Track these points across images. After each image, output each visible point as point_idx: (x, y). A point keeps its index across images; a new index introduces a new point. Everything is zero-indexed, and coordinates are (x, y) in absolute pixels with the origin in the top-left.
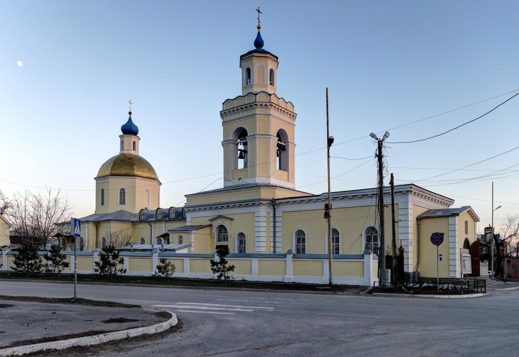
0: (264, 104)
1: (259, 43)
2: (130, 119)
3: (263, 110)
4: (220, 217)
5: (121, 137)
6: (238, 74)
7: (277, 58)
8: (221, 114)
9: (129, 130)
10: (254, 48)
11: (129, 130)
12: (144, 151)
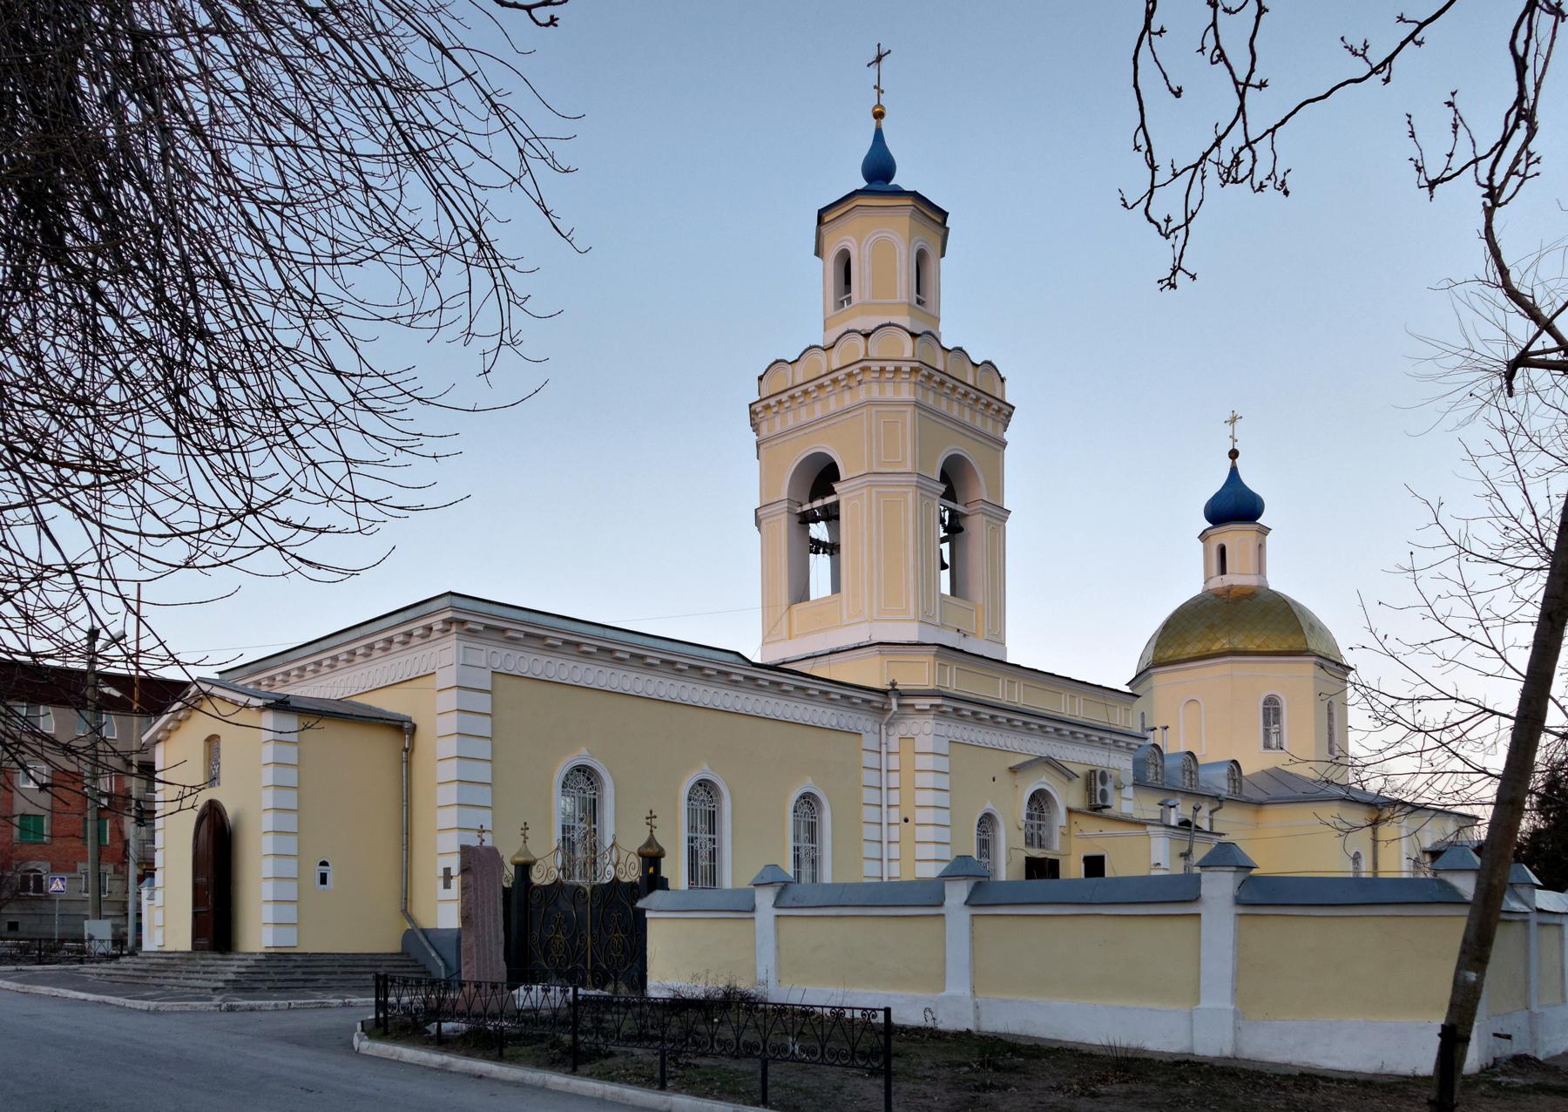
0: (890, 367)
1: (879, 169)
2: (1234, 471)
3: (889, 387)
4: (1049, 762)
5: (1203, 537)
6: (817, 275)
7: (945, 214)
8: (753, 413)
9: (1235, 508)
10: (862, 183)
11: (1235, 508)
12: (1289, 568)
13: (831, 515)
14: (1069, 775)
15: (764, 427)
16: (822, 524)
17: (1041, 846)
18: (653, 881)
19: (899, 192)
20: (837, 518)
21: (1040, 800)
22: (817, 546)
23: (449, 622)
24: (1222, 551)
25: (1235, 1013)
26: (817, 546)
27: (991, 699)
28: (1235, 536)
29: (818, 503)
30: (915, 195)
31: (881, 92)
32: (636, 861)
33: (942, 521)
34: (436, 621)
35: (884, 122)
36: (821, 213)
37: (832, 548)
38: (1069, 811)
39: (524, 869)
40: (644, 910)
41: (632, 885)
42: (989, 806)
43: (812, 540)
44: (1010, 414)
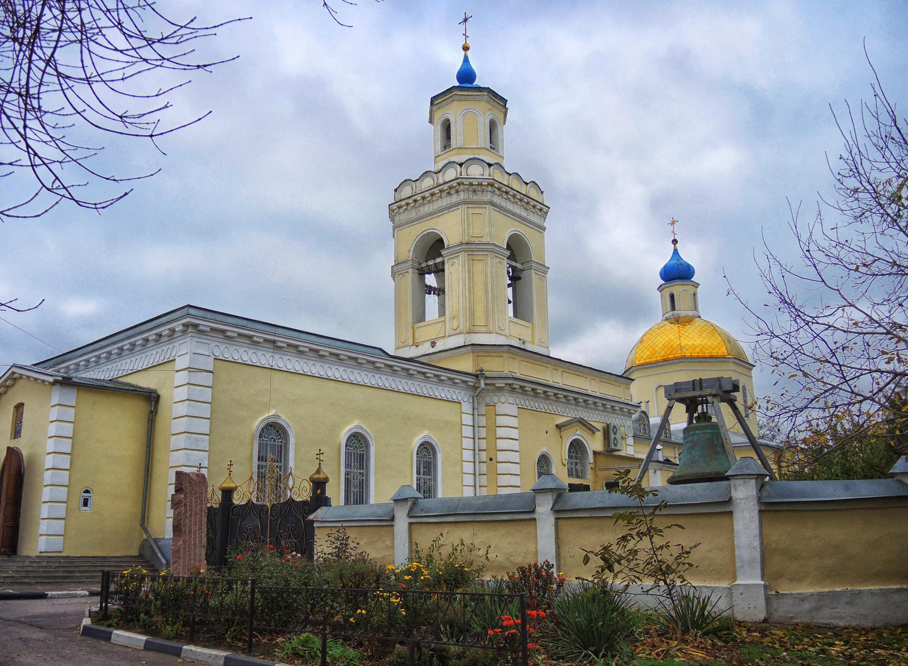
5: (660, 289)
8: (391, 211)
13: (439, 271)
14: (592, 430)
15: (397, 219)
16: (433, 275)
17: (577, 477)
18: (320, 499)
19: (479, 89)
20: (443, 270)
21: (577, 447)
22: (429, 290)
23: (186, 325)
24: (672, 297)
25: (765, 587)
26: (429, 290)
27: (540, 387)
28: (677, 288)
29: (431, 263)
30: (488, 90)
31: (466, 37)
32: (308, 486)
33: (508, 273)
34: (178, 326)
35: (469, 53)
36: (433, 99)
37: (440, 291)
38: (595, 453)
39: (228, 493)
40: (312, 522)
41: (304, 503)
42: (544, 449)
43: (427, 286)
44: (546, 213)
